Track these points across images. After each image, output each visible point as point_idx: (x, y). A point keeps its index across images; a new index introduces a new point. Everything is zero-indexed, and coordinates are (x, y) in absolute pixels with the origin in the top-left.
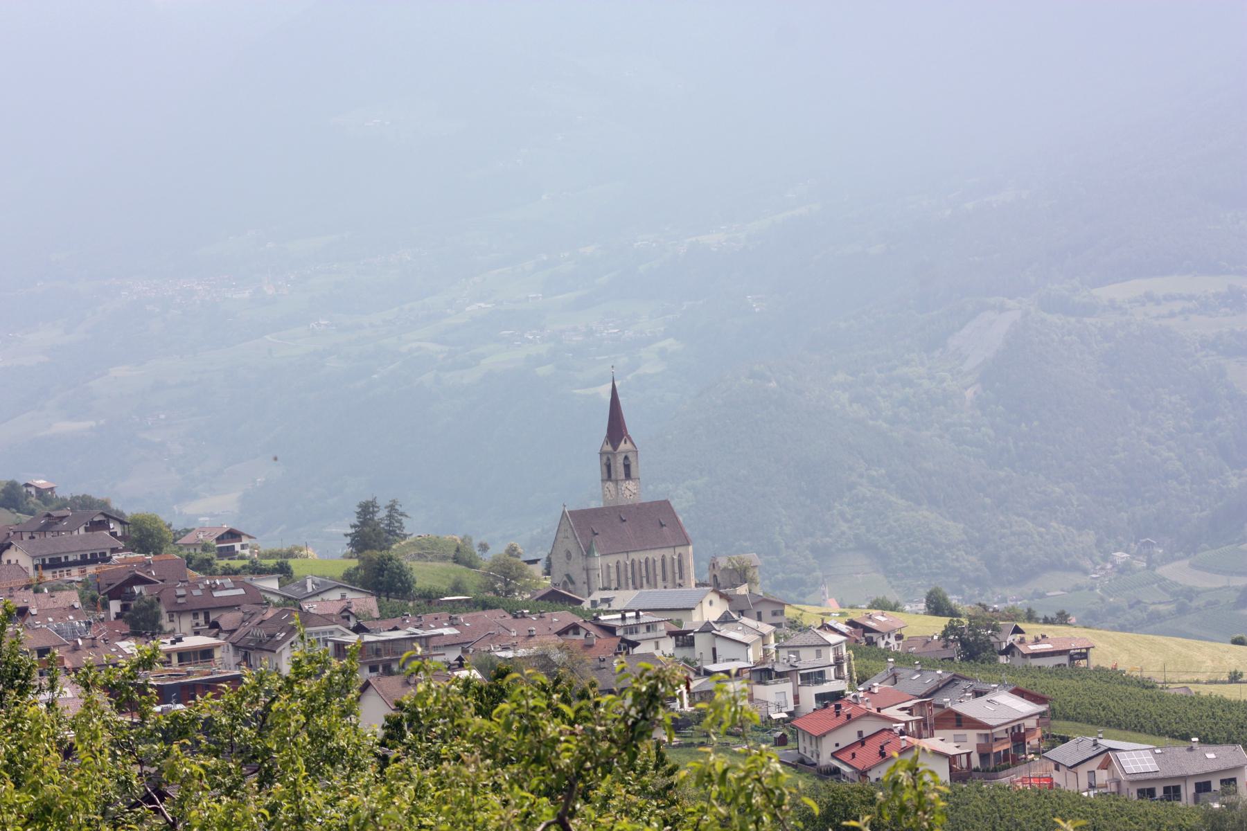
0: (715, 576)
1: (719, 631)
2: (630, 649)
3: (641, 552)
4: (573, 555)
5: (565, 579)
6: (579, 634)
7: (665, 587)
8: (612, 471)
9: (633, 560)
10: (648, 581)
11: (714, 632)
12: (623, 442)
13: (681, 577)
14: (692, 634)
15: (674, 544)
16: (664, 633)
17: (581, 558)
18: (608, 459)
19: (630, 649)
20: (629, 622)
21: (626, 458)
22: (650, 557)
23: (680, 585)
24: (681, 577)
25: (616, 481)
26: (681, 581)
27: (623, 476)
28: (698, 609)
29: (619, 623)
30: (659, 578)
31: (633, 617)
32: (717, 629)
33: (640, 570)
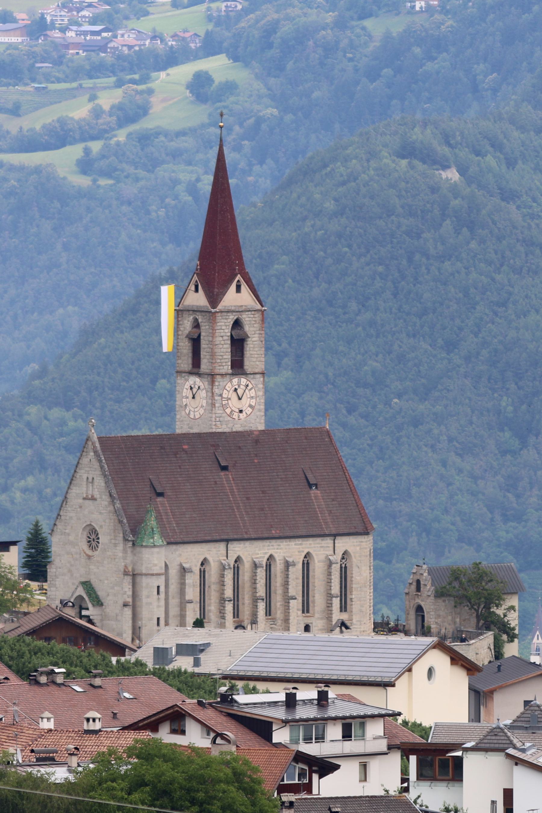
0: (419, 609)
1: (523, 751)
2: (315, 777)
3: (259, 544)
4: (103, 539)
5: (81, 591)
6: (183, 732)
7: (307, 628)
8: (204, 354)
9: (238, 560)
10: (268, 612)
11: (511, 751)
12: (233, 287)
13: (344, 608)
14: (459, 753)
15: (334, 532)
16: (383, 745)
17: (120, 547)
18: (197, 325)
19: (315, 777)
20: (302, 712)
21: (237, 324)
22: (279, 557)
23: (344, 625)
24: (344, 608)
25: (212, 376)
26: (344, 616)
27: (227, 368)
28: (401, 683)
29: (280, 713)
30: (296, 605)
31: (311, 701)
32: (519, 745)
33: (254, 582)
